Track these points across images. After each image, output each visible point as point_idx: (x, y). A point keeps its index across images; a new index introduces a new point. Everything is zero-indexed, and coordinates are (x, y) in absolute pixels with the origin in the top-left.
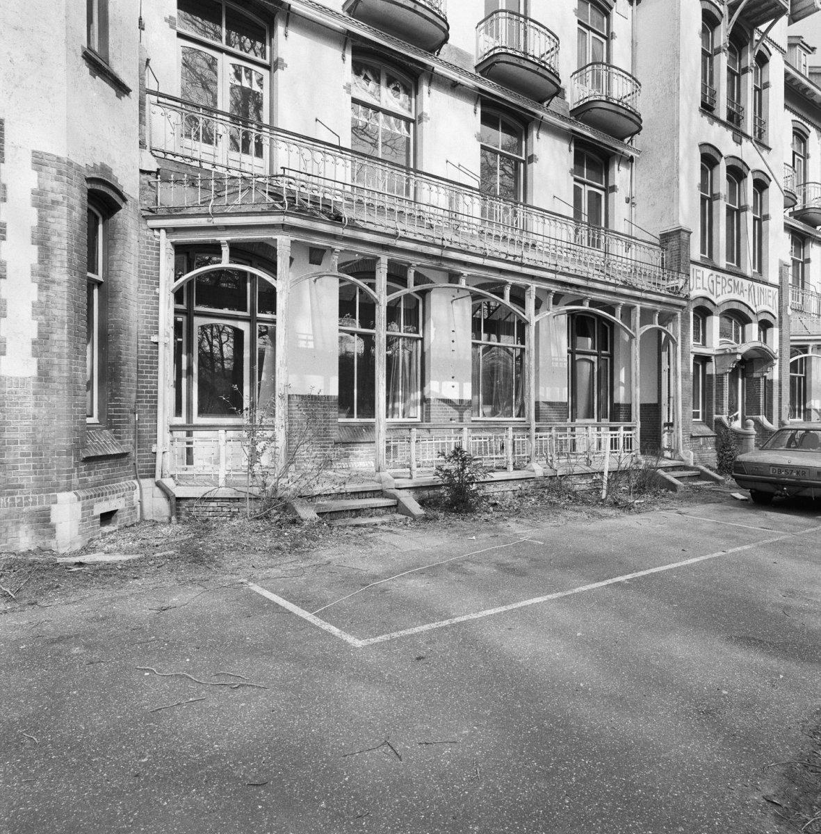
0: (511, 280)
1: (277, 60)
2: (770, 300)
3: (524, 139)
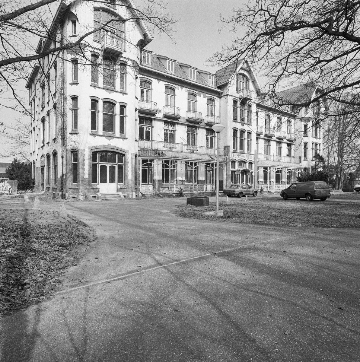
0: (190, 161)
2: (252, 158)
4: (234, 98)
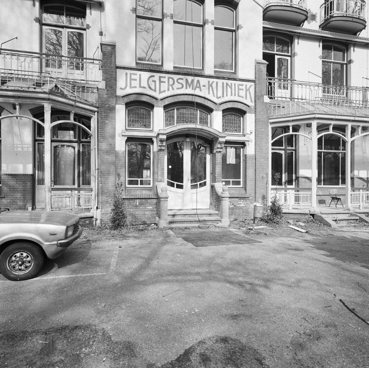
1: (351, 60)
3: (346, 52)
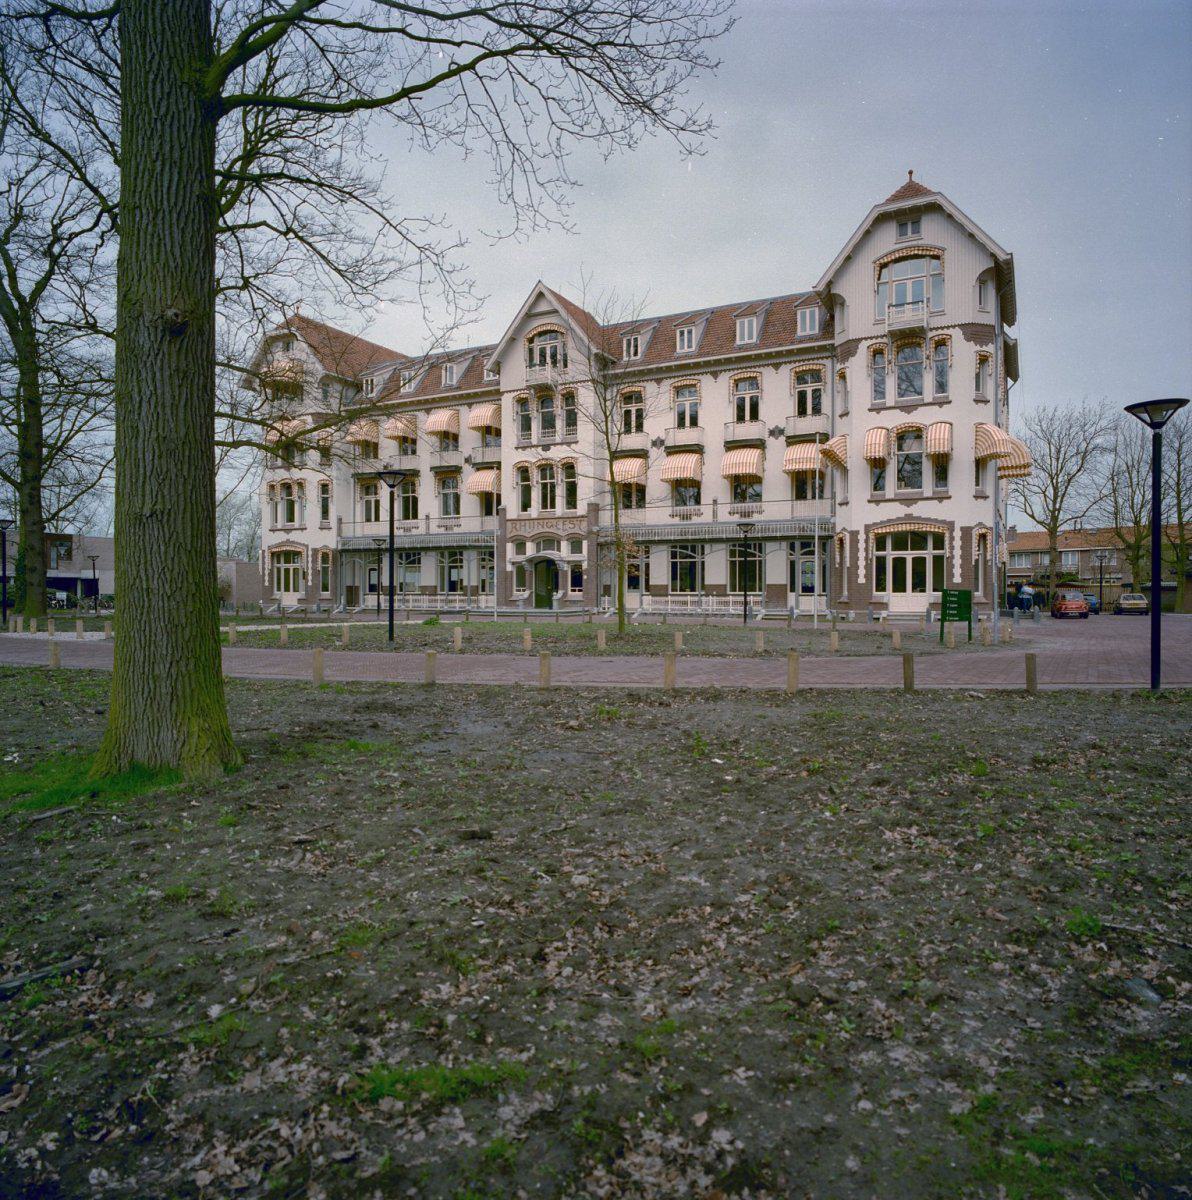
4: (870, 342)
